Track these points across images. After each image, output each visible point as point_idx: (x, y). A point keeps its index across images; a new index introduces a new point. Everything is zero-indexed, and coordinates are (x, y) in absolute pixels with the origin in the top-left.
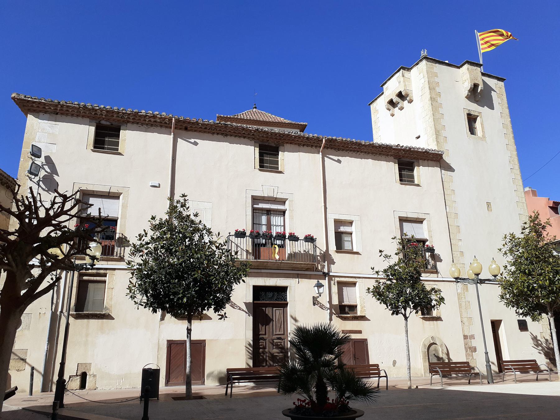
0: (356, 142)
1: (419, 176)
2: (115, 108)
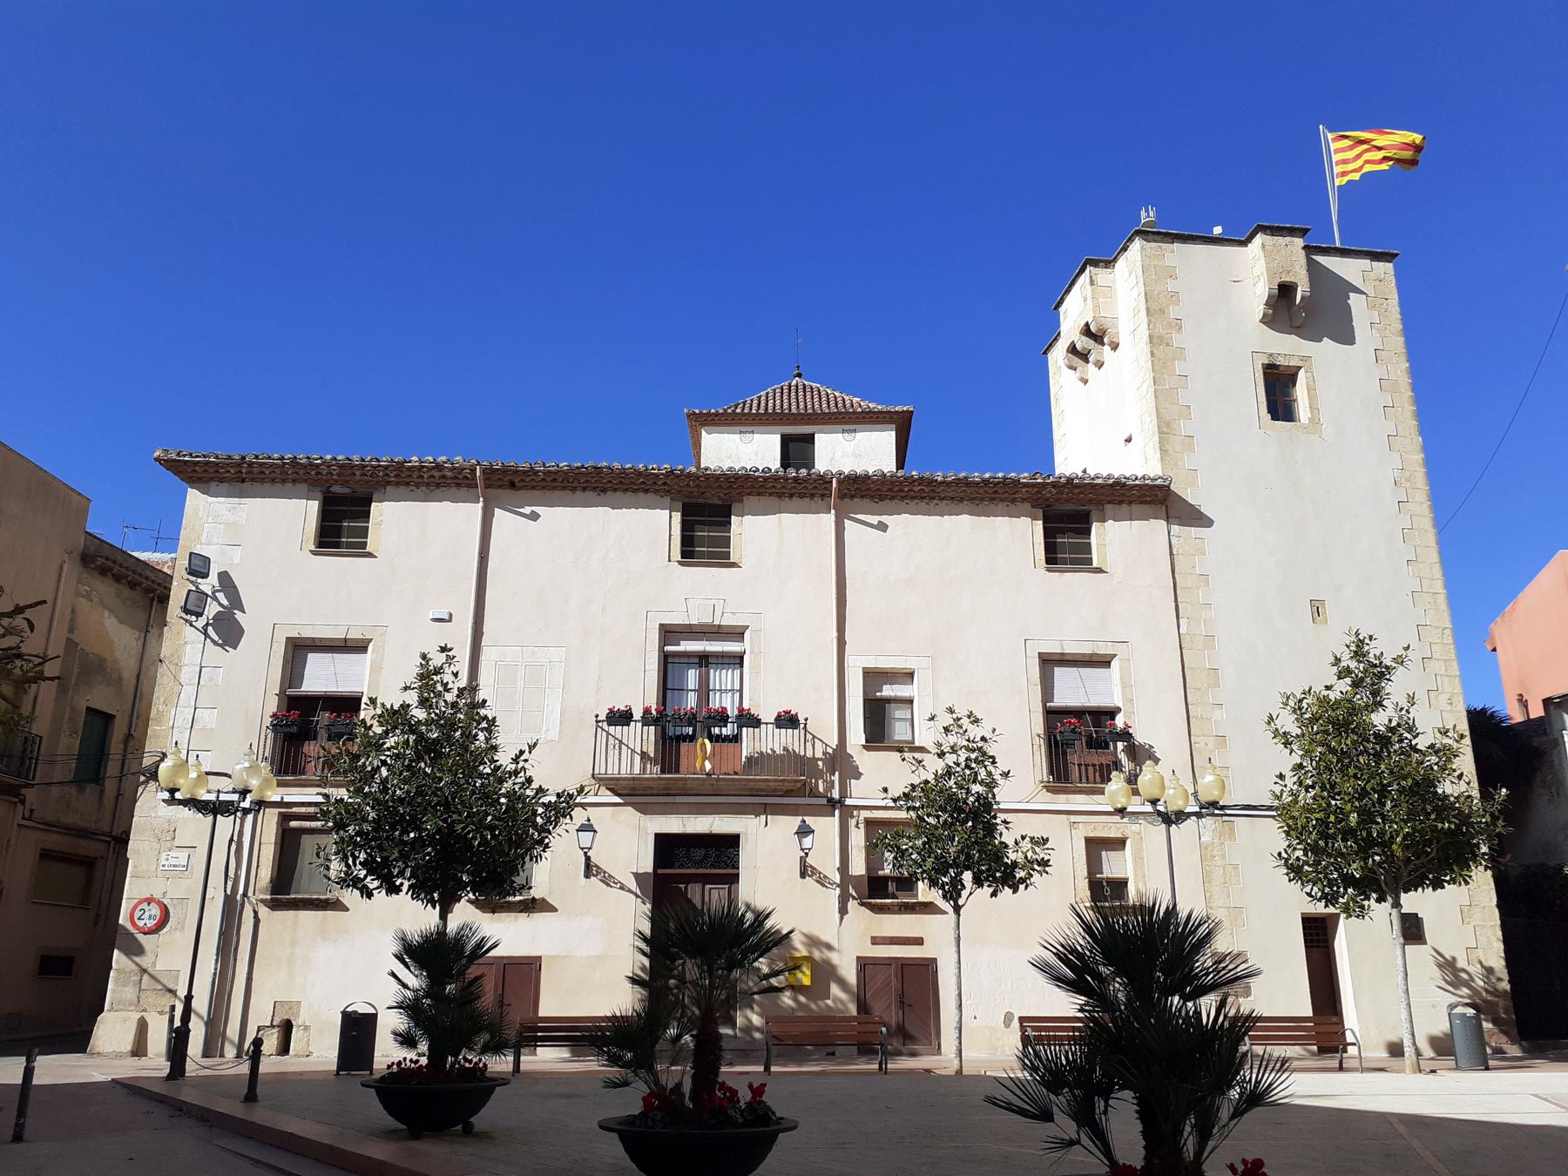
0: (921, 479)
1: (1102, 546)
2: (355, 458)
